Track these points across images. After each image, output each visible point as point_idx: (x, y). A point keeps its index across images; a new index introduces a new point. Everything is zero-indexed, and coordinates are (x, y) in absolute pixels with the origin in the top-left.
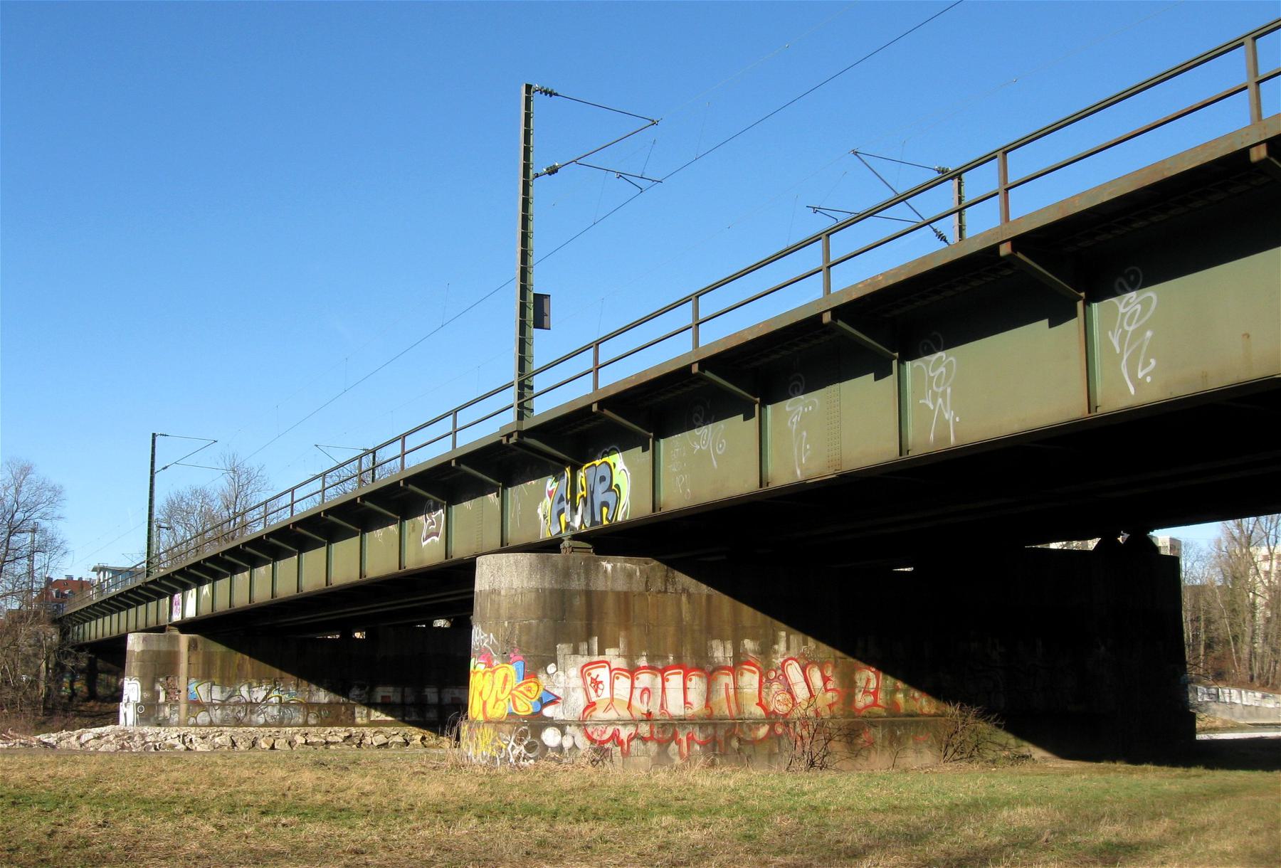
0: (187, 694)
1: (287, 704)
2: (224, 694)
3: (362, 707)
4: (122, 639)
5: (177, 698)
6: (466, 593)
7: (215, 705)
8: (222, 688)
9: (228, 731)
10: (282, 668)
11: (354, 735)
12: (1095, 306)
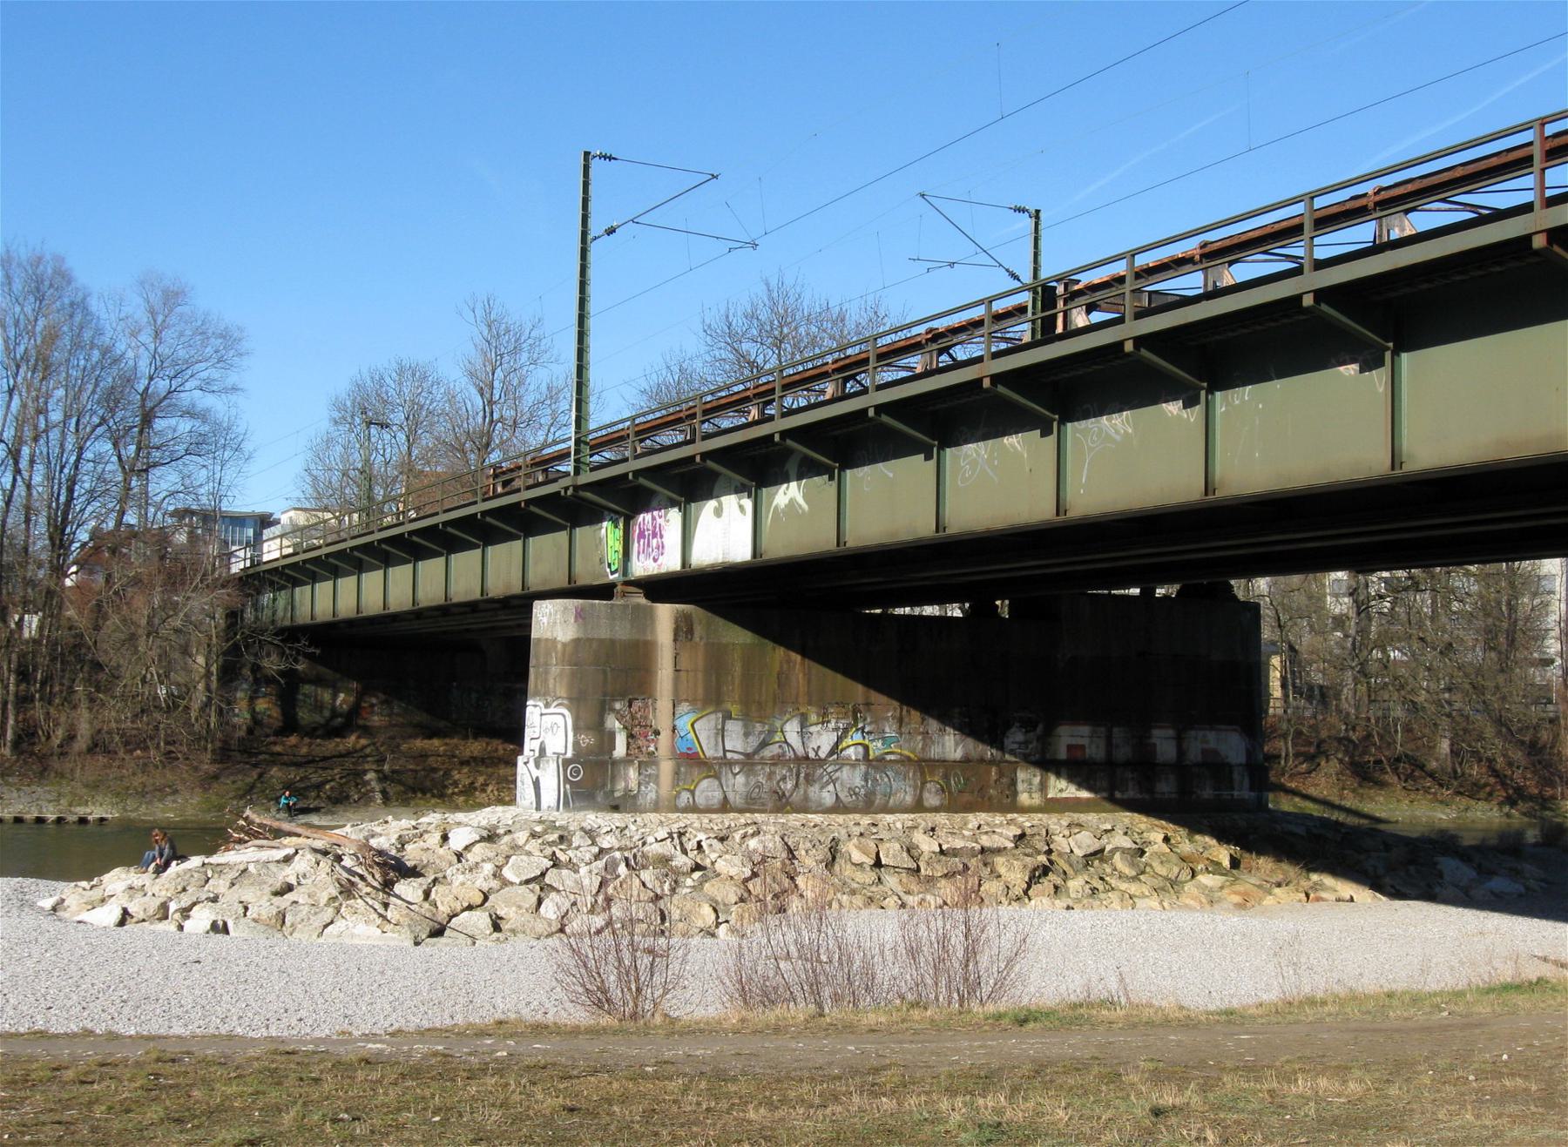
0: (673, 738)
1: (879, 764)
2: (751, 739)
3: (1032, 770)
4: (519, 606)
5: (652, 748)
6: (523, 618)
7: (731, 764)
8: (745, 726)
9: (771, 823)
10: (870, 682)
11: (1028, 832)
12: (1405, 356)
